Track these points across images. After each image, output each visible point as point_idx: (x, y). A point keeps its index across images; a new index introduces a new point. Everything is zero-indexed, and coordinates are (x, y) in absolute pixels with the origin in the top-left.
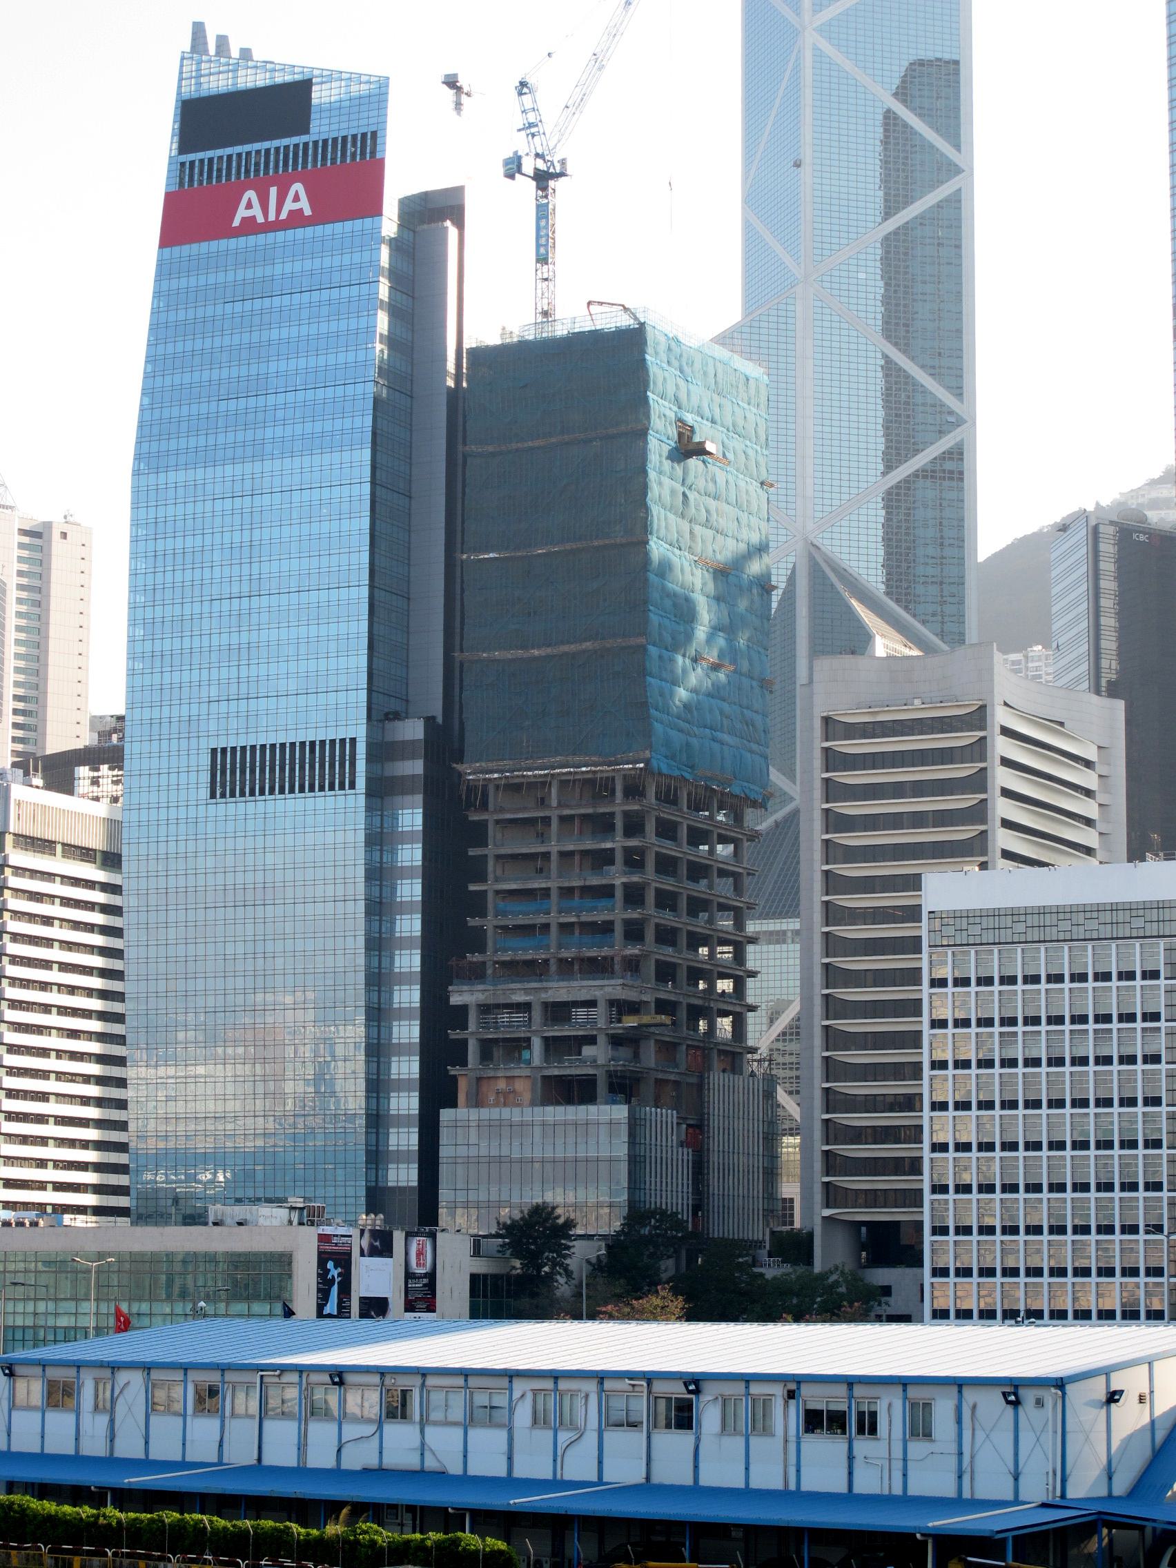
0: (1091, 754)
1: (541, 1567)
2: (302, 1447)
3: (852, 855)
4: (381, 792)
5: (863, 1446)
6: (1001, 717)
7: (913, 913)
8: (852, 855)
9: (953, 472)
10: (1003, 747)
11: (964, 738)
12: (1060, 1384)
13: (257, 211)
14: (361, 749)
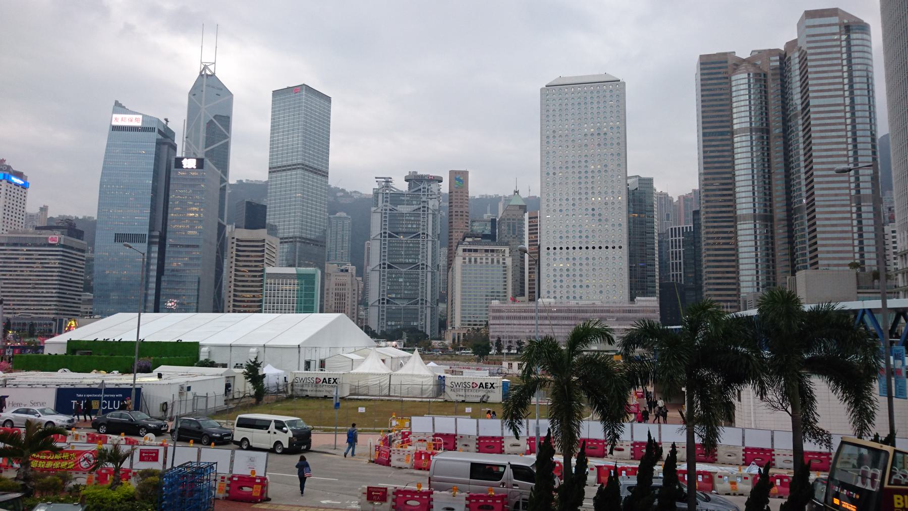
4: (150, 243)
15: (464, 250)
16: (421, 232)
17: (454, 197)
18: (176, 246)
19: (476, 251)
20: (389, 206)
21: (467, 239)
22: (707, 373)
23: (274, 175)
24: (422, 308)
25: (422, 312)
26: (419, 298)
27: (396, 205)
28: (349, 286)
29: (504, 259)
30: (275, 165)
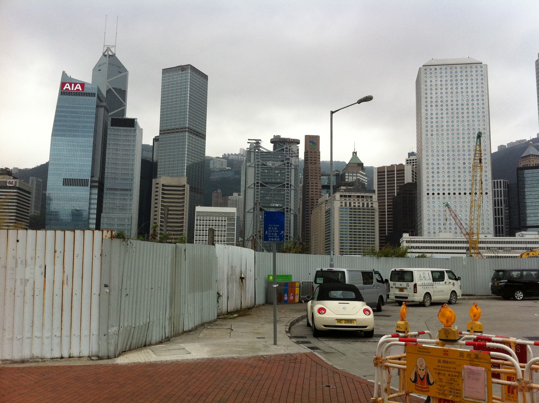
1: (538, 146)
3: (165, 202)
4: (92, 187)
8: (165, 202)
11: (181, 200)
13: (69, 88)
14: (89, 181)
15: (341, 196)
16: (286, 183)
17: (309, 156)
18: (111, 189)
30: (165, 128)
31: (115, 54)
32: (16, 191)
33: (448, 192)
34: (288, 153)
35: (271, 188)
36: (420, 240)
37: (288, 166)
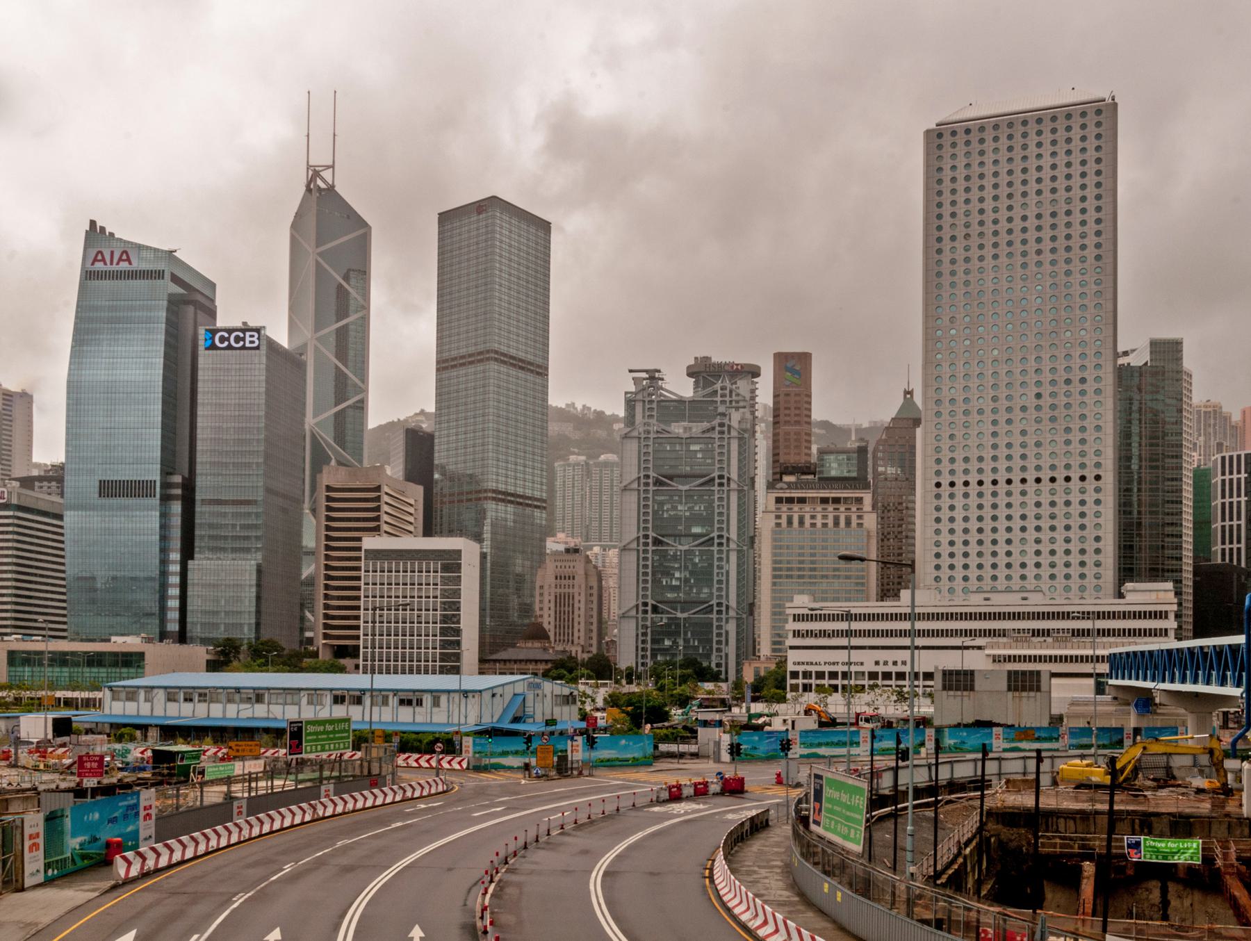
0: (412, 502)
2: (224, 711)
4: (166, 499)
5: (418, 709)
6: (386, 489)
7: (359, 549)
9: (361, 406)
10: (386, 498)
12: (480, 691)
14: (158, 484)
16: (716, 474)
19: (802, 500)
20: (655, 426)
21: (787, 478)
22: (891, 470)
23: (445, 375)
24: (719, 620)
25: (720, 627)
26: (714, 602)
27: (668, 422)
28: (580, 579)
29: (860, 517)
30: (446, 355)
31: (333, 186)
32: (11, 513)
33: (1050, 474)
34: (728, 399)
35: (681, 487)
36: (894, 611)
37: (723, 433)
